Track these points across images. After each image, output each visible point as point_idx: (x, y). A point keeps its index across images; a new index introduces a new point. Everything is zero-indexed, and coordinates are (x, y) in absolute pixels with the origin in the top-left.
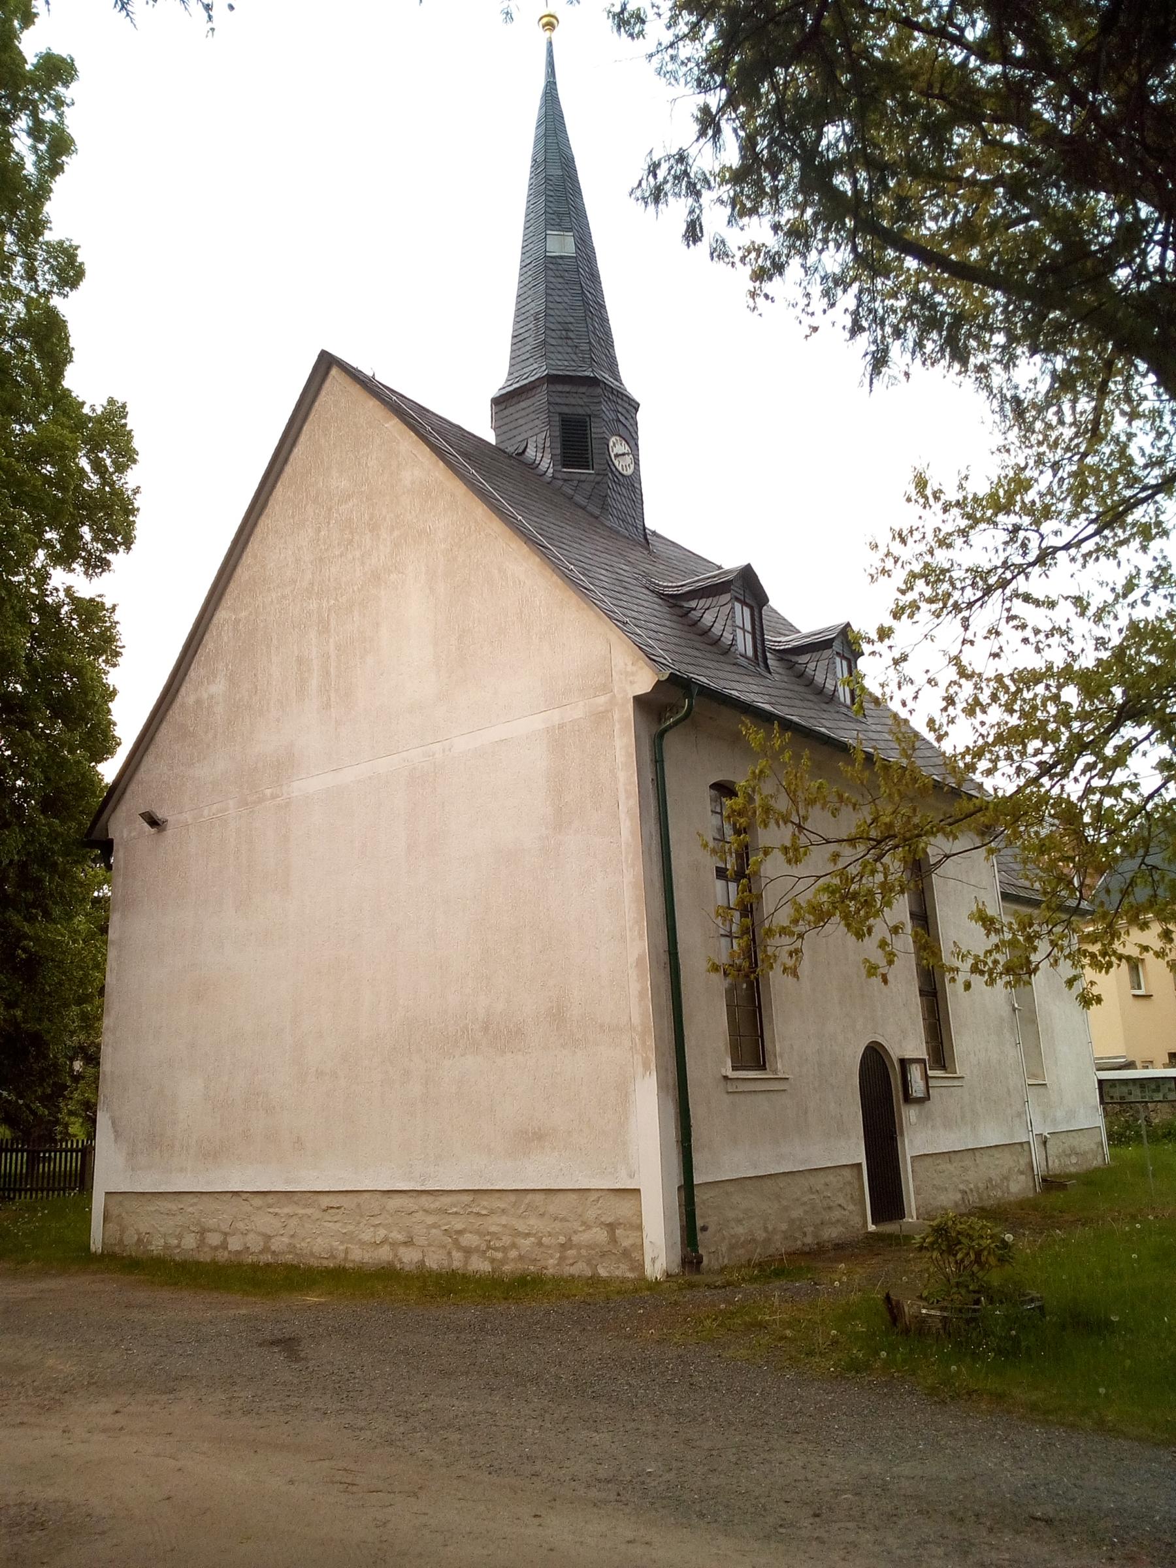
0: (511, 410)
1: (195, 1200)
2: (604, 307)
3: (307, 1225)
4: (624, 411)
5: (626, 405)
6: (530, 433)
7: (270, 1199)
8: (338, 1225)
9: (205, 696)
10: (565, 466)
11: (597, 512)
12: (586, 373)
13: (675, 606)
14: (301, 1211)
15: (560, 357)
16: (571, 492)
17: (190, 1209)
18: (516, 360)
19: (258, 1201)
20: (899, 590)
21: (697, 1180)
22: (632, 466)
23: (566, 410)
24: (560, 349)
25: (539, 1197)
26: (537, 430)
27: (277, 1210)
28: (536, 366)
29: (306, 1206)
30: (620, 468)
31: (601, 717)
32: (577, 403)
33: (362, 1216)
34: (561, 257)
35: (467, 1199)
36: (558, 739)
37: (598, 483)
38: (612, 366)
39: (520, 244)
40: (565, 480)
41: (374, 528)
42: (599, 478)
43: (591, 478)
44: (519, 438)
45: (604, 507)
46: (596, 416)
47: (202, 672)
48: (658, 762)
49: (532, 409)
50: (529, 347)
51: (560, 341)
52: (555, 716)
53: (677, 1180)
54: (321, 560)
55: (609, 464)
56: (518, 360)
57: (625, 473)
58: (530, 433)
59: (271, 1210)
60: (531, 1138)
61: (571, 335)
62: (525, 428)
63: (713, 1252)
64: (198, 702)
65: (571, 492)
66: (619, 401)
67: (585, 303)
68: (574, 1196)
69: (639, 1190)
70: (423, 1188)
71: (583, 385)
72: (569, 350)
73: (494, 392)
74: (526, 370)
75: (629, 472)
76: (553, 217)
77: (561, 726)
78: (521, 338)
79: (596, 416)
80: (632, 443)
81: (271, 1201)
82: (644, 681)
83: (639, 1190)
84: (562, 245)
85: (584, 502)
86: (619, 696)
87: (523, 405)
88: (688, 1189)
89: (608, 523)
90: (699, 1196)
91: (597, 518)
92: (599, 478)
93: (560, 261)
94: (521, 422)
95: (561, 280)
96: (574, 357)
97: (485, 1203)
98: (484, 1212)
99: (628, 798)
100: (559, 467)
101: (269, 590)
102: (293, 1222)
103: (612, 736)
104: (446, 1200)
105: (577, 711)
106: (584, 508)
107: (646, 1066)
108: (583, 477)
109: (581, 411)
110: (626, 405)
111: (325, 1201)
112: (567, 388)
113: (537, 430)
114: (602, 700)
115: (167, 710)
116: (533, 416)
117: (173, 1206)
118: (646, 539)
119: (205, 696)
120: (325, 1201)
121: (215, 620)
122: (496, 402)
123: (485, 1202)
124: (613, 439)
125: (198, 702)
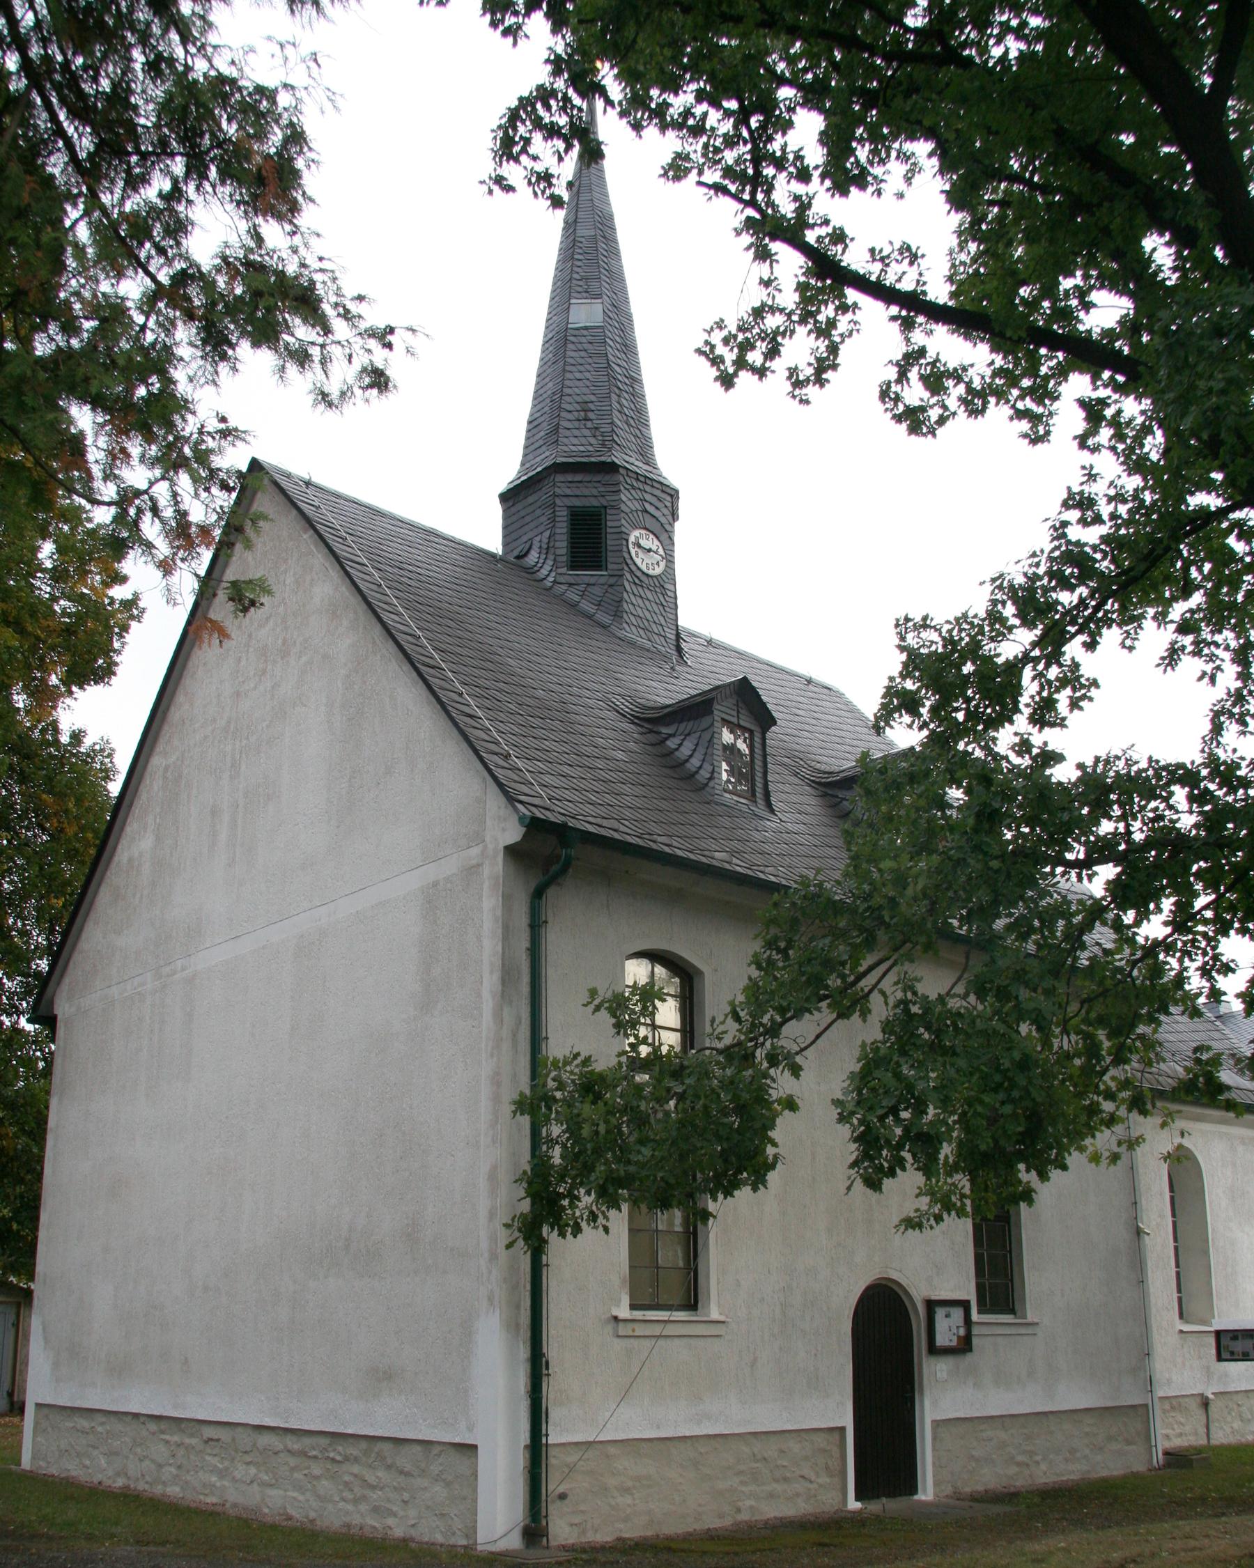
0: (519, 506)
1: (104, 1419)
2: (640, 382)
3: (192, 1457)
4: (654, 500)
5: (658, 493)
6: (536, 532)
7: (163, 1425)
8: (217, 1459)
9: (136, 855)
10: (572, 568)
11: (606, 620)
12: (603, 459)
13: (651, 731)
14: (187, 1441)
15: (575, 441)
16: (577, 598)
17: (100, 1429)
18: (530, 448)
19: (153, 1426)
20: (1222, 671)
21: (555, 1435)
22: (663, 565)
23: (577, 502)
24: (576, 432)
25: (386, 1447)
26: (542, 528)
27: (167, 1437)
28: (547, 453)
29: (192, 1435)
30: (643, 568)
31: (472, 871)
32: (587, 493)
33: (236, 1451)
34: (586, 328)
35: (324, 1441)
36: (432, 899)
37: (611, 586)
38: (645, 449)
39: (544, 316)
40: (571, 585)
41: (284, 654)
42: (612, 580)
43: (603, 580)
44: (525, 538)
45: (618, 614)
46: (613, 507)
47: (135, 825)
48: (536, 926)
49: (539, 504)
50: (542, 434)
51: (576, 424)
52: (432, 872)
53: (524, 1438)
54: (238, 694)
55: (627, 562)
56: (533, 447)
57: (651, 572)
58: (536, 532)
59: (164, 1437)
60: (382, 1377)
61: (591, 415)
62: (532, 525)
63: (563, 1529)
64: (130, 860)
65: (577, 598)
66: (648, 488)
67: (611, 377)
68: (418, 1448)
69: (475, 1447)
70: (286, 1426)
71: (599, 472)
72: (587, 433)
73: (503, 486)
74: (538, 459)
75: (658, 571)
76: (580, 283)
77: (435, 884)
78: (536, 423)
79: (613, 507)
80: (664, 537)
81: (163, 1427)
82: (513, 833)
83: (475, 1447)
84: (586, 313)
85: (591, 609)
86: (491, 847)
87: (531, 499)
88: (536, 1449)
89: (621, 634)
90: (555, 1461)
91: (605, 627)
92: (612, 580)
93: (585, 332)
94: (528, 519)
95: (583, 354)
96: (593, 441)
97: (340, 1448)
98: (338, 1458)
99: (491, 972)
100: (564, 570)
101: (194, 731)
102: (182, 1452)
103: (480, 898)
104: (307, 1441)
105: (450, 867)
106: (590, 617)
107: (490, 1299)
108: (592, 580)
109: (595, 503)
110: (658, 493)
111: (209, 1432)
112: (578, 477)
113: (542, 528)
114: (475, 851)
115: (106, 870)
116: (539, 512)
117: (84, 1423)
118: (679, 650)
119: (136, 855)
120: (209, 1432)
121: (149, 768)
122: (505, 498)
123: (342, 1448)
124: (636, 533)
125: (130, 860)
